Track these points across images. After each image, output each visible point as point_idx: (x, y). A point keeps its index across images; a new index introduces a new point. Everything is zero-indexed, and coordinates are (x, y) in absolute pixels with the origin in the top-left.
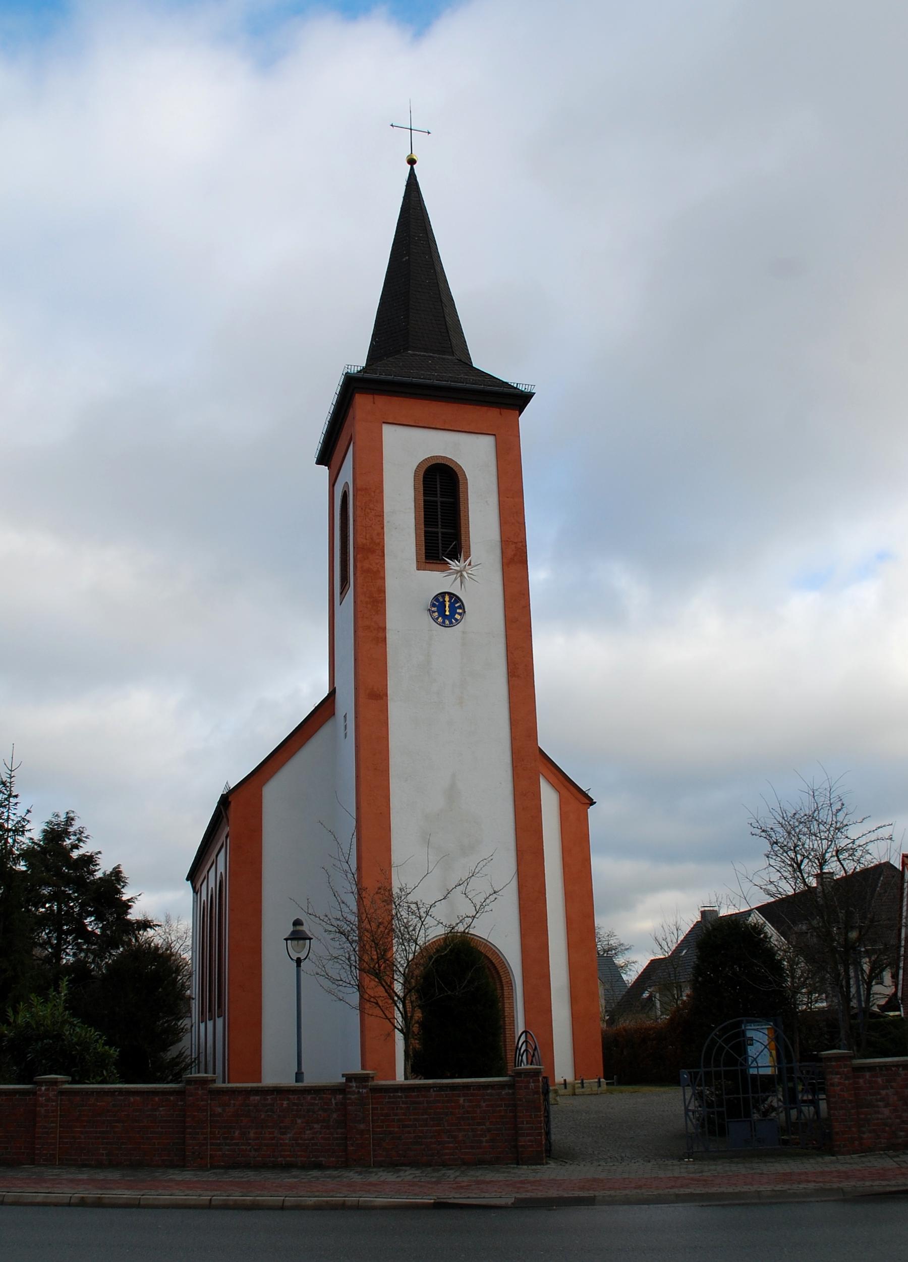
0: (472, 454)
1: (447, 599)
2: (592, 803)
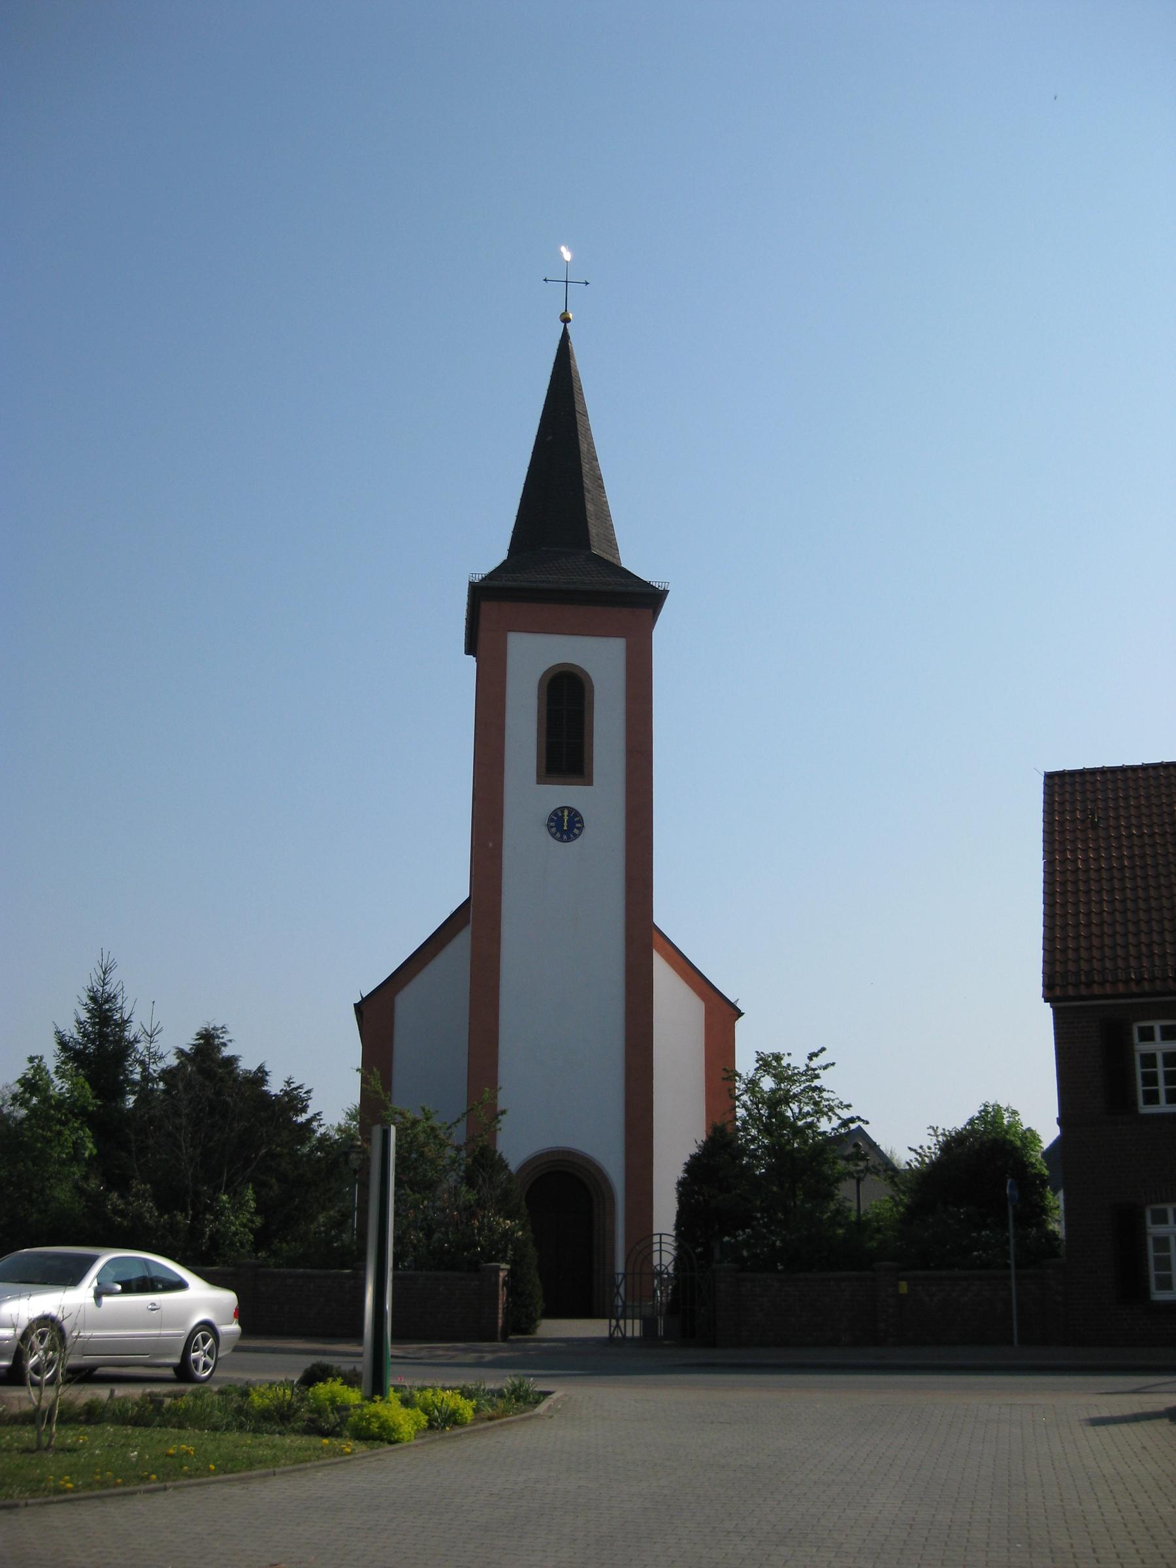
0: (599, 657)
1: (566, 813)
2: (740, 1014)
